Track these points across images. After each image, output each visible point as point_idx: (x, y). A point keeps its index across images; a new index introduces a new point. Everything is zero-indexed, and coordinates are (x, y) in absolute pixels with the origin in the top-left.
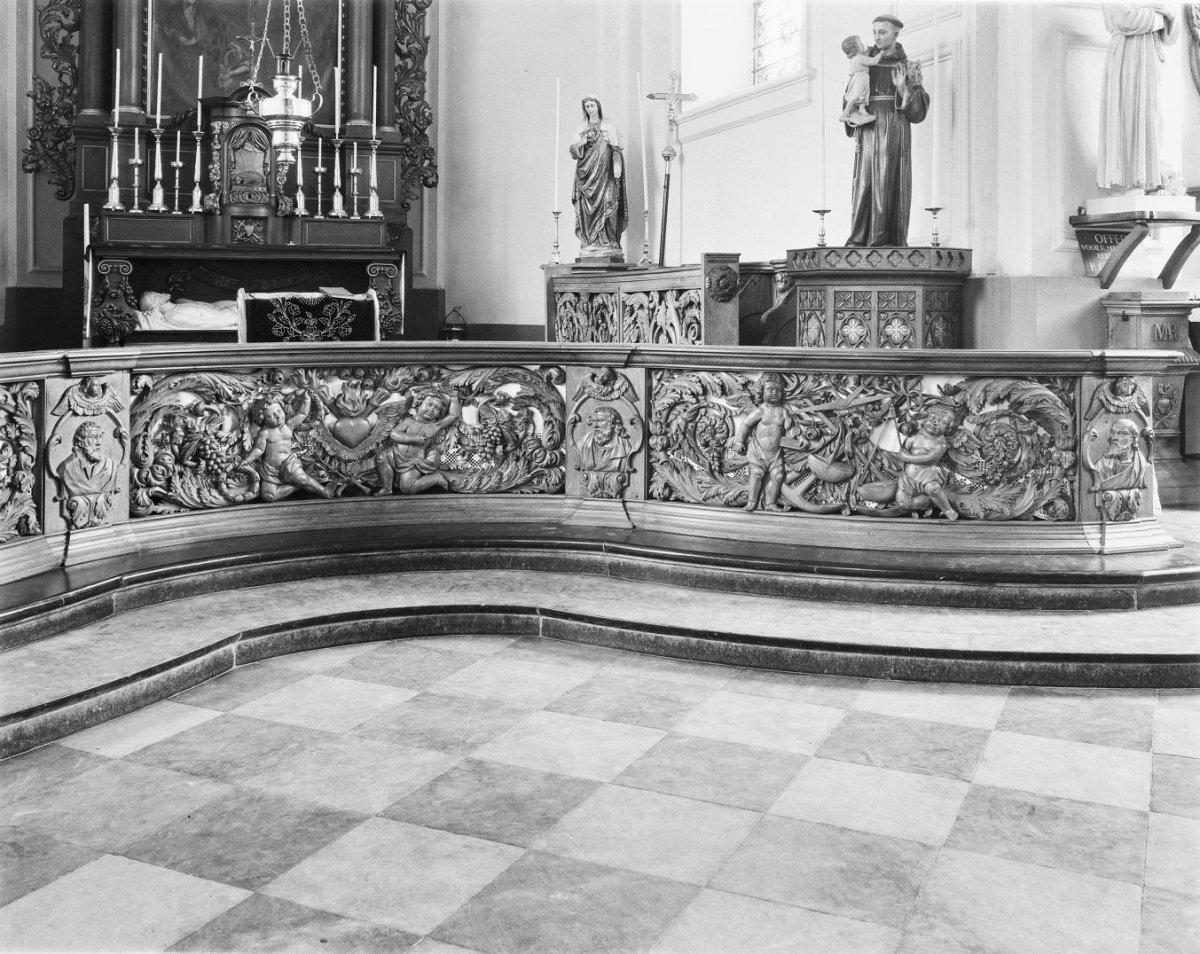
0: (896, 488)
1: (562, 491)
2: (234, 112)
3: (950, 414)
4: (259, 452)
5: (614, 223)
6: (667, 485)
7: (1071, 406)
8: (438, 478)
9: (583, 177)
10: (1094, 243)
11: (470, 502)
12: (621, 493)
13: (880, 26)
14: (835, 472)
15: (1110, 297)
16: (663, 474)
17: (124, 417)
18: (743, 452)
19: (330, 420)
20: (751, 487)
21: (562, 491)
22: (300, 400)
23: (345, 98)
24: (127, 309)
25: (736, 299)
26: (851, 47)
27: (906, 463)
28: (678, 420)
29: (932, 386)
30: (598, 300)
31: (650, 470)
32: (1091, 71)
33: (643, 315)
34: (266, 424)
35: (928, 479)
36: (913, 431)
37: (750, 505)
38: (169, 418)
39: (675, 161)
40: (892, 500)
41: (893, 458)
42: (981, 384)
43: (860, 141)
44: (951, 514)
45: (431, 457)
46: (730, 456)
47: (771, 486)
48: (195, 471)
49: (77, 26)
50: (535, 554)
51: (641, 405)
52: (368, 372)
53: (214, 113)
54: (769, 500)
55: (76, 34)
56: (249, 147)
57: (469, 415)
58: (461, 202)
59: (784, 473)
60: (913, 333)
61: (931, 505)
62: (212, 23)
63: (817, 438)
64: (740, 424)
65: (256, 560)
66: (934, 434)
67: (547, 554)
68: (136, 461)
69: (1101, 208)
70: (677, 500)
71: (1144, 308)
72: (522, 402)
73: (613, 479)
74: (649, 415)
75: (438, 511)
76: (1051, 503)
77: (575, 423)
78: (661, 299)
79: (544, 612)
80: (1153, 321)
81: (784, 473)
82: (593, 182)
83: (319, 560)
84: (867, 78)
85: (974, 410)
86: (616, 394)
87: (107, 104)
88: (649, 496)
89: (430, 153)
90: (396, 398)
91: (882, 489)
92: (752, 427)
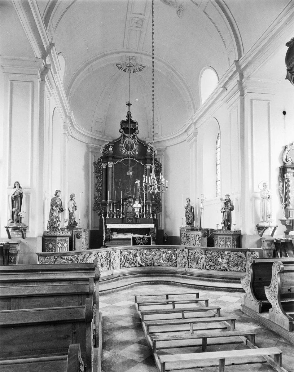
0: (221, 267)
1: (176, 266)
2: (127, 201)
3: (228, 257)
4: (136, 260)
5: (192, 220)
6: (191, 266)
7: (246, 256)
8: (159, 264)
9: (187, 212)
10: (260, 229)
11: (164, 267)
12: (185, 267)
13: (226, 196)
14: (213, 264)
15: (262, 238)
16: (190, 264)
17: (119, 255)
18: (201, 261)
19: (145, 256)
20: (202, 266)
21: (176, 266)
22: (141, 253)
23: (146, 197)
24: (111, 235)
25: (206, 237)
26: (221, 200)
27: (223, 263)
28: (192, 256)
29: (226, 253)
30: (187, 235)
31: (188, 264)
32: (259, 202)
33: (194, 238)
34: (136, 256)
35: (226, 265)
36: (223, 259)
37: (202, 269)
38: (124, 256)
39: (202, 209)
40: (220, 268)
41: (221, 263)
42: (233, 252)
43: (223, 214)
44: (228, 270)
45: (159, 261)
46: (199, 262)
47: (204, 266)
48: (128, 262)
49: (101, 186)
50: (172, 275)
51: (187, 254)
52: (150, 250)
53: (124, 201)
54: (204, 268)
55: (101, 187)
56: (130, 207)
57: (164, 255)
58: (166, 216)
59: (206, 264)
60: (231, 243)
61: (226, 269)
62: (123, 185)
63: (210, 260)
64: (200, 257)
65: (136, 274)
66: (226, 259)
67: (174, 275)
68: (121, 261)
69: (261, 224)
70: (192, 268)
71: (266, 240)
72: (171, 254)
73: (183, 265)
74: (188, 256)
75: (160, 269)
76: (243, 269)
77: (178, 257)
78: (196, 236)
79: (172, 282)
80: (267, 242)
81: (206, 264)
82: (188, 213)
83: (144, 275)
84: (224, 204)
85: (232, 256)
86: (184, 253)
87: (106, 199)
88: (188, 267)
89: (161, 205)
90: (154, 253)
91: (219, 267)
92: (202, 258)
